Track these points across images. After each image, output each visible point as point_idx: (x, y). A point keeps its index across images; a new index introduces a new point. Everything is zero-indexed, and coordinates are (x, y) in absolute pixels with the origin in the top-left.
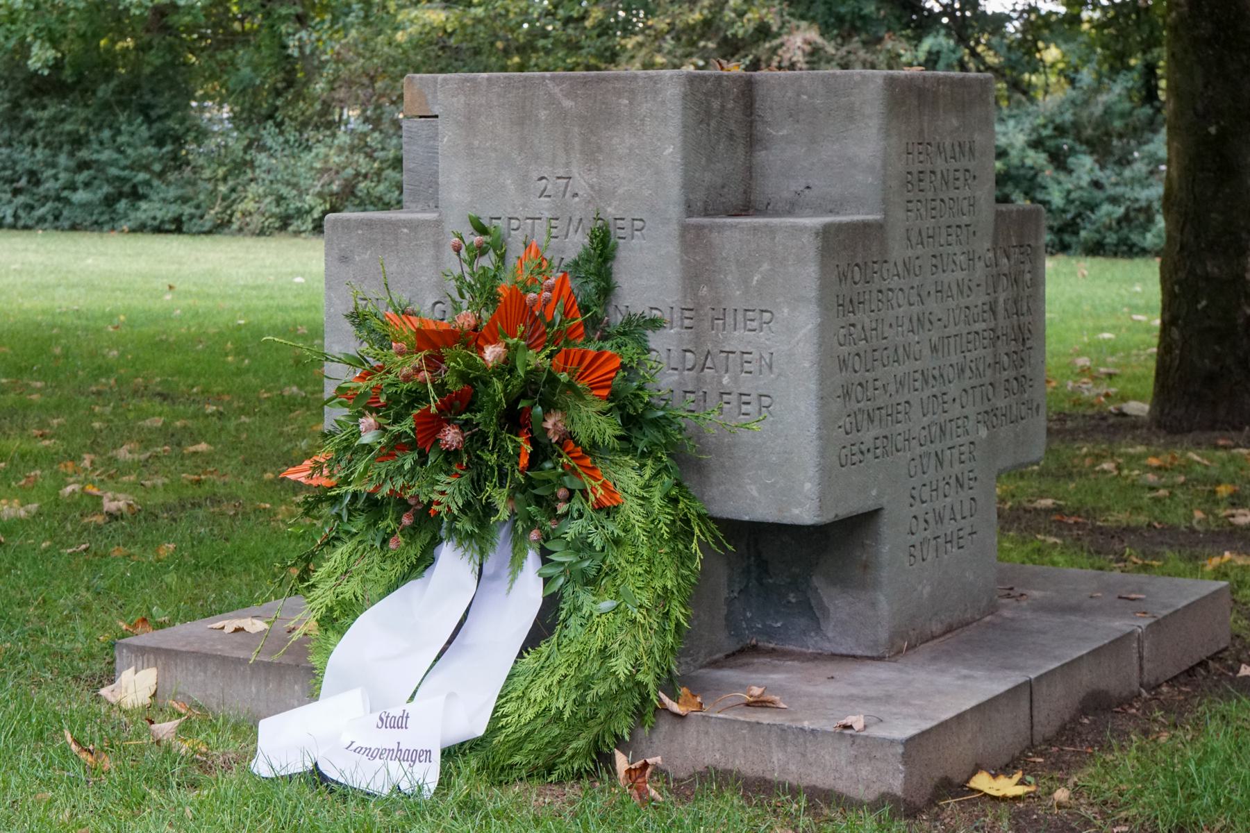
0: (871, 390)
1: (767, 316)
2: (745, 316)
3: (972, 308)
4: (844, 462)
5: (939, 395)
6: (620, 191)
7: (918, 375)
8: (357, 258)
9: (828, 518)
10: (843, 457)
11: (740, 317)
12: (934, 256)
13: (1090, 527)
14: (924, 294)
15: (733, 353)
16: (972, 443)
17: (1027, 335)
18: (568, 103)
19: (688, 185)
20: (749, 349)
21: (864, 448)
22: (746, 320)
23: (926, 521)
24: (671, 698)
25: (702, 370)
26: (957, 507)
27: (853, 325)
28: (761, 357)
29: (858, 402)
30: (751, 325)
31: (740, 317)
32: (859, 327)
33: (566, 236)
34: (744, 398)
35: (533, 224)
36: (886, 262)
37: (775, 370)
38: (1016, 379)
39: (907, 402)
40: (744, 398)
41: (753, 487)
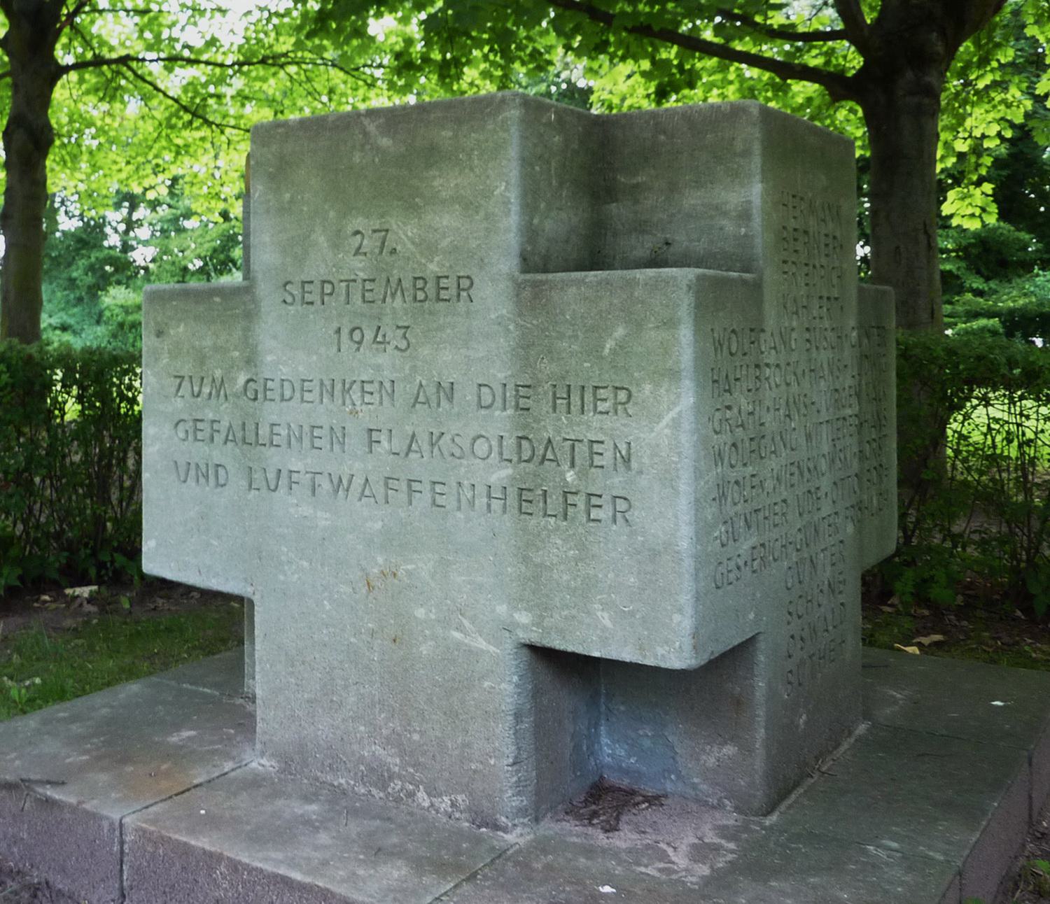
0: (748, 488)
1: (622, 396)
2: (595, 395)
3: (841, 391)
4: (720, 584)
5: (813, 490)
6: (444, 243)
7: (794, 469)
8: (172, 332)
9: (703, 659)
10: (719, 577)
11: (588, 397)
12: (808, 329)
13: (544, 384)
14: (799, 372)
15: (202, 421)
16: (841, 542)
17: (883, 422)
18: (385, 142)
19: (530, 233)
20: (601, 437)
21: (741, 563)
22: (596, 399)
23: (802, 639)
24: (704, 275)
25: (542, 462)
26: (829, 617)
27: (729, 408)
28: (616, 447)
29: (735, 504)
30: (602, 406)
31: (588, 397)
32: (735, 410)
33: (384, 301)
34: (594, 501)
35: (348, 286)
36: (763, 331)
37: (634, 465)
38: (875, 468)
39: (784, 501)
40: (594, 501)
41: (606, 615)
